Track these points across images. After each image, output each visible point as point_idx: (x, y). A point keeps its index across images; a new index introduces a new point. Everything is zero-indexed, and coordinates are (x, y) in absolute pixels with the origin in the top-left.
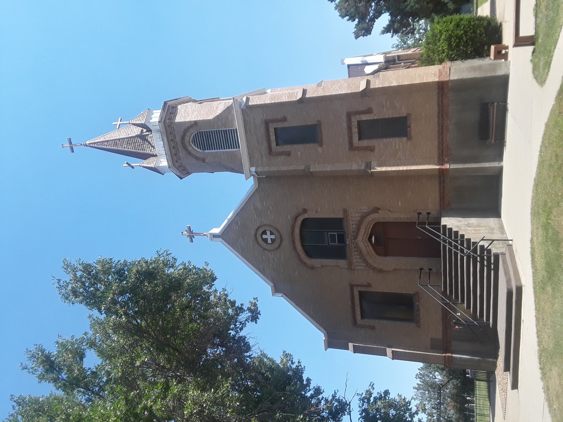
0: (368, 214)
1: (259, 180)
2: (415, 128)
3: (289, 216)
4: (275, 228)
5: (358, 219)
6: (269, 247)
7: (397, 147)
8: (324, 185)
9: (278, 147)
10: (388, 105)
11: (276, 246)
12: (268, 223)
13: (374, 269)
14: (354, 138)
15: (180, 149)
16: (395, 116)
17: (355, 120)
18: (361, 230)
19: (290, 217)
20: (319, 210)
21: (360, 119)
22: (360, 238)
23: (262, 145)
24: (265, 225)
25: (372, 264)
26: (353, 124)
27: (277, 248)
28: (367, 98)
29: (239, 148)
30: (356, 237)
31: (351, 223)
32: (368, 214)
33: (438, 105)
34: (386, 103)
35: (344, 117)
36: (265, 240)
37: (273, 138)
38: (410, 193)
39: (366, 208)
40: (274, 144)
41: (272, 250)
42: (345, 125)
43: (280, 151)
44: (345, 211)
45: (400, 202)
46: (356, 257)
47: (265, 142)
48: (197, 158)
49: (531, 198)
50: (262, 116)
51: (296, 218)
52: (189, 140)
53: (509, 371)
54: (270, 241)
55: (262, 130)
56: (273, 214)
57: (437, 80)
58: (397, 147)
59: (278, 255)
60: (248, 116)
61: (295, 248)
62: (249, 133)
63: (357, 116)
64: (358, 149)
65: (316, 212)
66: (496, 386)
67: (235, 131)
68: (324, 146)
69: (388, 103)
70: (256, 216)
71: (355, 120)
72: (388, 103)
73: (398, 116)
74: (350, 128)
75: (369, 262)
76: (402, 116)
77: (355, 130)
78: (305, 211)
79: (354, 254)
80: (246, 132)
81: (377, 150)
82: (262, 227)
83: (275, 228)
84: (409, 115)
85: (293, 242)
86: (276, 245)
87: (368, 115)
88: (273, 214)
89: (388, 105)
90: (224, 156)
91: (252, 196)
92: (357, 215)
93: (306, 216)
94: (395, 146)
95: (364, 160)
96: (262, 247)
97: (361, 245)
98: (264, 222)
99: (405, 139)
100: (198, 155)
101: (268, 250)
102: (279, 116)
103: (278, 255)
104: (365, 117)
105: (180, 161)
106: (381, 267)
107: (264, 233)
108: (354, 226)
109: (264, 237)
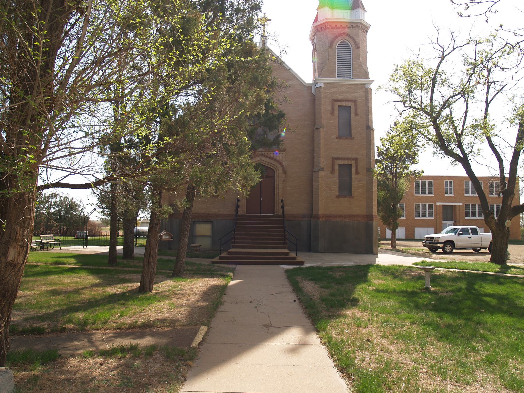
1: (309, 86)
5: (278, 159)
9: (337, 107)
15: (339, 30)
16: (352, 188)
17: (353, 163)
18: (269, 160)
21: (352, 165)
22: (264, 158)
23: (339, 95)
26: (350, 161)
28: (366, 172)
30: (264, 155)
35: (355, 156)
37: (344, 104)
40: (340, 104)
44: (284, 150)
48: (332, 43)
53: (228, 255)
55: (351, 98)
63: (355, 165)
64: (333, 164)
68: (336, 140)
70: (49, 99)
73: (353, 190)
74: (348, 159)
77: (345, 162)
80: (349, 84)
81: (331, 175)
84: (353, 197)
91: (297, 79)
92: (281, 158)
94: (333, 188)
99: (337, 194)
100: (334, 44)
102: (359, 111)
104: (353, 169)
105: (330, 28)
108: (272, 155)
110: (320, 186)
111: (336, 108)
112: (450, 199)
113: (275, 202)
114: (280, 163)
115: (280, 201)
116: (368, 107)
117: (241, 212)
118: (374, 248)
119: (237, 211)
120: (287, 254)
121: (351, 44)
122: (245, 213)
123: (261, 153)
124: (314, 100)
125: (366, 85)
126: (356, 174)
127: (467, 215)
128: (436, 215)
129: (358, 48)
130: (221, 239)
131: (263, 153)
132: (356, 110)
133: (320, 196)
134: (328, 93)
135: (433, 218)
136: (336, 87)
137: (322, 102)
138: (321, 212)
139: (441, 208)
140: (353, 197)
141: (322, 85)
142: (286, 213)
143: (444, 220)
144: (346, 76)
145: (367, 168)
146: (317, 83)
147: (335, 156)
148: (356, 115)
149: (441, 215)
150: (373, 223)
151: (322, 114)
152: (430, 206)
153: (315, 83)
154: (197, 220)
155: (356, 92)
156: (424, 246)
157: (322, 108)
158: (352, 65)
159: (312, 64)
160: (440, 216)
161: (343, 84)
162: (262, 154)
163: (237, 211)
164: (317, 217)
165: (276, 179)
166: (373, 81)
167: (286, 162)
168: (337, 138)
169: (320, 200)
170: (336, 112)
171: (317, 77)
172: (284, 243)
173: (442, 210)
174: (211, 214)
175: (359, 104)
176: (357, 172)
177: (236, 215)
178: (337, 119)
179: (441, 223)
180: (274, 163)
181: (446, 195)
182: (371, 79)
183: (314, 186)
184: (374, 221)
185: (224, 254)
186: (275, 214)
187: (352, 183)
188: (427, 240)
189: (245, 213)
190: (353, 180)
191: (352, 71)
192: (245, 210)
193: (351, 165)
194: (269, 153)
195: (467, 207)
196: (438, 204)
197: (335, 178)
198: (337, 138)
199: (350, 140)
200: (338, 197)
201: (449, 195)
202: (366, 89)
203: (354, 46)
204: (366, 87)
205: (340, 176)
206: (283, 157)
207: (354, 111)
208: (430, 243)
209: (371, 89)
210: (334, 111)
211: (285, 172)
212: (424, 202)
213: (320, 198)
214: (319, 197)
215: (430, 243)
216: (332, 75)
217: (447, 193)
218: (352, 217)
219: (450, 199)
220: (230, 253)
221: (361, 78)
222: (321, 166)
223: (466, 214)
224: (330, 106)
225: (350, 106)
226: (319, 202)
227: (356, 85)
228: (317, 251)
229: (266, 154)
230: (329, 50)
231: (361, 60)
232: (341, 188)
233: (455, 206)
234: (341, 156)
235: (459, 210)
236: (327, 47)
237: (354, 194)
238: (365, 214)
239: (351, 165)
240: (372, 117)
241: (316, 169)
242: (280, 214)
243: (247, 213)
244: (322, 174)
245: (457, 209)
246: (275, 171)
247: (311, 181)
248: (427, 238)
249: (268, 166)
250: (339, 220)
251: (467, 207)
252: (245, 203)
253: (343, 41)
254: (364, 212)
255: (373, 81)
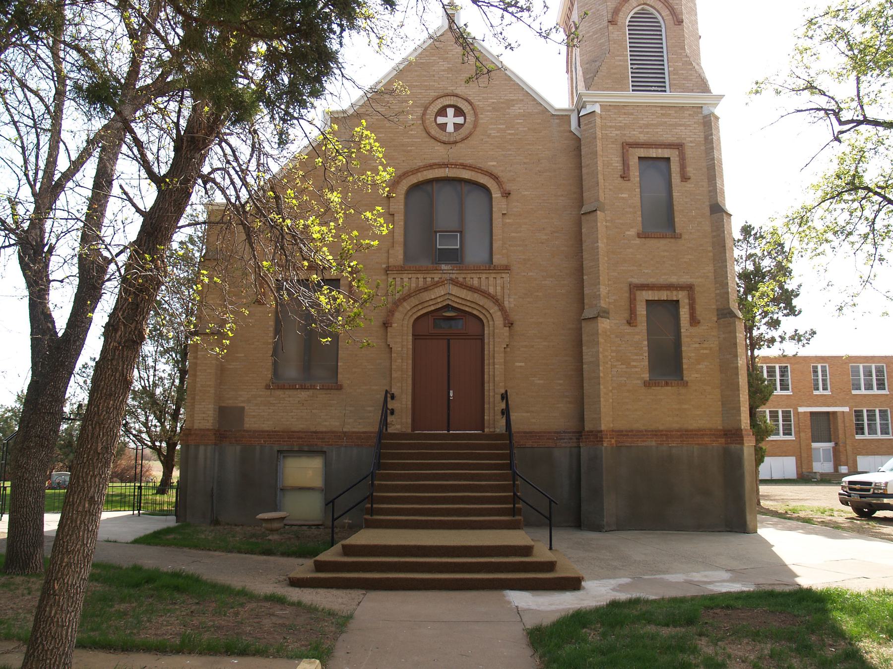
0: (502, 309)
1: (563, 117)
2: (666, 394)
3: (495, 163)
4: (470, 134)
5: (491, 290)
6: (430, 117)
7: (634, 364)
8: (556, 234)
9: (637, 160)
10: (702, 351)
11: (433, 132)
12: (481, 121)
13: (391, 312)
14: (650, 292)
16: (684, 361)
17: (681, 296)
19: (493, 165)
20: (508, 221)
22: (455, 290)
23: (640, 133)
24: (476, 115)
25: (400, 308)
26: (675, 293)
27: (428, 133)
28: (715, 319)
29: (633, 90)
30: (455, 282)
31: (484, 276)
32: (502, 309)
33: (699, 430)
34: (706, 349)
35: (685, 279)
36: (442, 112)
37: (653, 153)
38: (539, 382)
39: (512, 305)
40: (643, 153)
41: (423, 122)
42: (674, 280)
43: (630, 163)
45: (523, 364)
46: (414, 280)
47: (645, 138)
48: (616, 11)
49: (814, 588)
50: (691, 139)
51: (495, 178)
52: (648, 5)
54: (440, 120)
56: (499, 134)
57: (743, 427)
58: (634, 364)
59: (413, 132)
60: (690, 115)
61: (431, 166)
62: (661, 112)
63: (687, 301)
64: (632, 301)
65: (503, 214)
66: (534, 562)
67: (663, 89)
68: (638, 241)
69: (705, 352)
71: (681, 296)
72: (705, 352)
73: (685, 367)
75: (405, 304)
76: (685, 372)
77: (664, 295)
78: (507, 194)
79: (419, 276)
81: (628, 329)
82: (473, 109)
83: (470, 134)
84: (685, 384)
85: (445, 165)
86: (434, 131)
87: (688, 319)
88: (499, 134)
89: (702, 351)
90: (620, 61)
92: (499, 288)
93: (496, 194)
94: (634, 360)
95: (612, 306)
96: (430, 104)
97: (440, 291)
98: (482, 114)
99: (646, 376)
101: (424, 114)
102: (690, 170)
103: (413, 132)
106: (395, 325)
107: (459, 112)
108: (476, 282)
109: (450, 112)
110: (601, 356)
111: (634, 162)
112: (824, 401)
113: (486, 400)
114: (497, 300)
115: (499, 397)
116: (713, 159)
117: (399, 427)
118: (749, 517)
119: (384, 422)
120: (527, 550)
121: (663, 16)
122: (409, 431)
123: (447, 276)
124: (578, 149)
125: (705, 107)
126: (691, 325)
127: (860, 429)
128: (799, 432)
129: (680, 22)
130: (333, 501)
131: (454, 276)
132: (683, 167)
133: (602, 381)
134: (611, 127)
135: (792, 438)
136: (632, 114)
137: (599, 148)
138: (606, 424)
139: (809, 415)
140: (685, 384)
141: (597, 109)
142: (514, 428)
143: (815, 440)
144: (656, 89)
145: (718, 310)
146: (583, 107)
147: (635, 281)
148: (685, 178)
149: (809, 431)
150: (742, 450)
151: (600, 177)
152: (787, 416)
153: (580, 105)
154: (285, 448)
155: (681, 125)
156: (844, 502)
157: (600, 163)
158: (666, 63)
159: (566, 77)
160: (807, 434)
161: (650, 106)
162: (451, 279)
163: (384, 422)
164: (597, 436)
165: (486, 341)
166: (722, 96)
167: (511, 300)
168: (639, 236)
169: (602, 394)
170: (635, 173)
171: (581, 88)
172: (514, 512)
173: (808, 422)
174: (322, 432)
175: (689, 153)
176: (694, 321)
177: (382, 434)
178: (638, 190)
179: (810, 449)
180: (483, 301)
181: (816, 393)
182: (715, 89)
183: (586, 358)
184: (746, 444)
185: (329, 555)
186: (486, 430)
187: (684, 348)
188: (851, 489)
189: (409, 431)
190: (684, 340)
191: (667, 76)
192: (409, 421)
193: (678, 301)
194: (469, 276)
195: (858, 414)
196: (801, 410)
197: (640, 334)
198: (639, 236)
199: (673, 240)
200: (647, 384)
201: (821, 392)
202: (705, 117)
203: (669, 18)
204: (705, 112)
205: (651, 331)
206: (503, 288)
207: (678, 169)
208: (862, 496)
209: (717, 118)
210: (628, 169)
211: (510, 324)
212: (774, 407)
213: (602, 387)
214: (599, 384)
215: (862, 496)
216: (618, 84)
217: (818, 389)
218: (686, 434)
219: (824, 401)
220: (348, 550)
221: (692, 91)
222: (603, 304)
223: (857, 429)
224: (619, 159)
225: (669, 159)
226: (599, 396)
227: (682, 108)
228: (597, 528)
229: (461, 279)
230: (611, 28)
231: (688, 51)
232: (654, 366)
233: (835, 413)
234: (651, 281)
235: (844, 422)
236: (605, 23)
237: (689, 375)
238: (720, 427)
239: (678, 301)
240: (723, 185)
241: (587, 313)
242: (498, 431)
243: (413, 430)
244: (604, 324)
245: (840, 420)
246: (485, 321)
247: (578, 345)
248: (850, 483)
249: (467, 309)
250: (654, 443)
251: (858, 414)
252: (410, 403)
253: (643, 9)
254: (716, 422)
255: (722, 96)
